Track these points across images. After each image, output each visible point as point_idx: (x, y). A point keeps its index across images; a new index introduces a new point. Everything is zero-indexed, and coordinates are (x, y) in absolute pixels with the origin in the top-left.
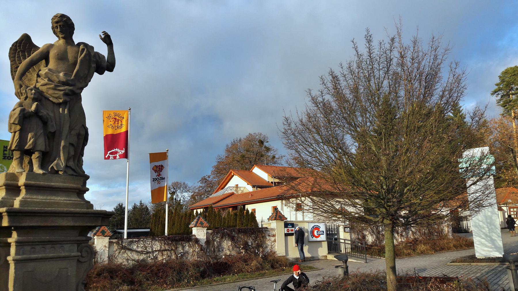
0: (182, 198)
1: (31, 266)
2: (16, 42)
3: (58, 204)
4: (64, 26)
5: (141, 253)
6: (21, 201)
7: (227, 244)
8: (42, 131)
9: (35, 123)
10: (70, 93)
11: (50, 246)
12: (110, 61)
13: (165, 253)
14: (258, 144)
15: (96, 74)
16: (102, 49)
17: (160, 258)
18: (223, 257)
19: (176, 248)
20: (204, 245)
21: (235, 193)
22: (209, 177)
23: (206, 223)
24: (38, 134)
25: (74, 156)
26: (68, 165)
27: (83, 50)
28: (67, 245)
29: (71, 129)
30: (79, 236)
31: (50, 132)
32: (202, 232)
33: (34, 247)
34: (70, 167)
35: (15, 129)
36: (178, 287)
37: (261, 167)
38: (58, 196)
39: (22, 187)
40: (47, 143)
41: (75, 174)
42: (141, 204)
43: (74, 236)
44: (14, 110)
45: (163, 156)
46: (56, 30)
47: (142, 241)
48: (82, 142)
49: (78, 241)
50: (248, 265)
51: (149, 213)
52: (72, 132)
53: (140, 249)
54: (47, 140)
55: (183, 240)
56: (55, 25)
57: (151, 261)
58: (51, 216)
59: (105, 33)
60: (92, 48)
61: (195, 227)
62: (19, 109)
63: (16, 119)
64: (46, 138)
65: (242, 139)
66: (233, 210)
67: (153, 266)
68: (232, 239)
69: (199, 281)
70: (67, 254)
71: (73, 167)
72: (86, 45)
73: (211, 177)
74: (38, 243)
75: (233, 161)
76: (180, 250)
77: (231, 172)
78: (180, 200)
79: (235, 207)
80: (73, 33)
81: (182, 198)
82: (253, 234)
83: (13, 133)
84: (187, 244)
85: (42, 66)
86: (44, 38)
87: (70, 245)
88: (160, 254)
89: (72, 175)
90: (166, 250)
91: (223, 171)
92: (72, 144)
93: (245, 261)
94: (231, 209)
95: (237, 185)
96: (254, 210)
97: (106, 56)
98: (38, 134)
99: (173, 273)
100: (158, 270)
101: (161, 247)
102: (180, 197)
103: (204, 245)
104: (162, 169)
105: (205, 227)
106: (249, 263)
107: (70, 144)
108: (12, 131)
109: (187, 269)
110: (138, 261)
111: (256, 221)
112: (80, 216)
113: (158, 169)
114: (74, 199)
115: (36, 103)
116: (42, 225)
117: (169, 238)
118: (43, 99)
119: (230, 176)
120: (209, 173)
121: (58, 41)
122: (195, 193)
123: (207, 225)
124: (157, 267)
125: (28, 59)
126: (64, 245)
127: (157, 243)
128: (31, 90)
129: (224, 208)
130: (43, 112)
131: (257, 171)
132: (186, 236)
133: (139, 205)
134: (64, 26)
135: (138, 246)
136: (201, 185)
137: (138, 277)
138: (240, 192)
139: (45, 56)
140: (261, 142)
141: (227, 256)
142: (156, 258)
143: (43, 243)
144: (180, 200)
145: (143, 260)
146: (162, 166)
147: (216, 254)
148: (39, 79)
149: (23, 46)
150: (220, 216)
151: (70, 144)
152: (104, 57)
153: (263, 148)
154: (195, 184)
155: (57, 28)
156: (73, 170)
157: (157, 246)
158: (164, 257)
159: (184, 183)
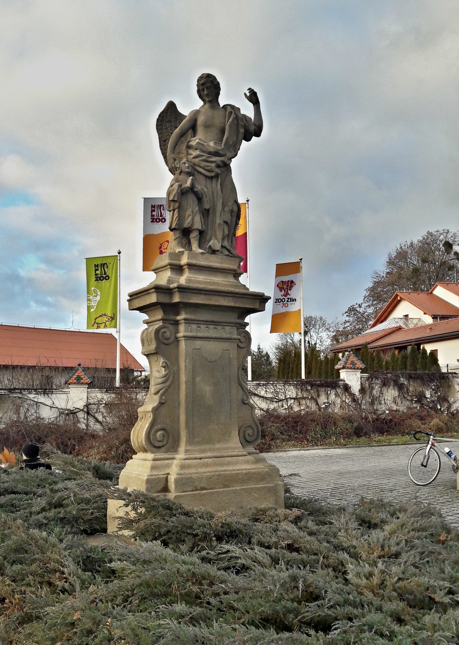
0: (318, 342)
1: (198, 344)
2: (163, 112)
3: (217, 284)
4: (209, 87)
5: (271, 400)
6: (186, 280)
7: (391, 393)
8: (197, 208)
9: (191, 200)
10: (221, 164)
11: (213, 326)
12: (257, 124)
13: (303, 402)
14: (443, 248)
15: (243, 141)
16: (248, 110)
17: (296, 409)
18: (387, 412)
19: (319, 396)
20: (357, 393)
21: (403, 326)
22: (360, 306)
23: (360, 364)
24: (195, 211)
25: (228, 235)
26: (223, 245)
27: (231, 113)
28: (228, 327)
29: (224, 205)
30: (238, 318)
31: (205, 209)
32: (355, 376)
33: (199, 325)
34: (225, 247)
35: (173, 206)
36: (323, 445)
37: (447, 286)
38: (217, 276)
39: (184, 267)
40: (203, 221)
41: (230, 255)
42: (259, 349)
43: (233, 318)
44: (171, 186)
45: (295, 267)
46: (202, 93)
47: (272, 384)
48: (235, 219)
49: (238, 323)
50: (425, 424)
51: (270, 364)
52: (226, 209)
53: (269, 395)
54: (202, 219)
55: (328, 386)
56: (201, 88)
57: (284, 411)
58: (214, 295)
59: (251, 90)
60: (239, 109)
61: (344, 368)
62: (177, 185)
63: (175, 195)
64: (202, 216)
65: (415, 242)
66: (399, 352)
67: (288, 416)
68: (400, 387)
69: (352, 440)
70: (228, 336)
71: (228, 248)
72: (233, 107)
73: (364, 305)
74: (202, 322)
75: (399, 278)
76: (322, 399)
77: (397, 295)
78: (315, 344)
79: (401, 347)
80: (219, 94)
81: (318, 342)
82: (432, 381)
83: (172, 212)
84: (333, 392)
85: (189, 136)
86: (190, 104)
87: (230, 327)
88: (296, 403)
89: (228, 255)
90: (304, 398)
91: (385, 296)
92: (226, 222)
93: (422, 418)
94: (396, 352)
95: (406, 316)
96: (434, 354)
97: (253, 118)
98: (195, 211)
99: (316, 427)
100: (295, 422)
101: (297, 394)
102: (315, 339)
103: (357, 393)
104: (291, 287)
105: (358, 369)
106: (427, 421)
107: (224, 222)
108: (171, 209)
109: (335, 423)
110: (267, 411)
111: (438, 365)
112: (240, 297)
113: (285, 287)
114: (231, 279)
115: (191, 177)
116: (207, 302)
117: (307, 383)
118: (196, 173)
119: (396, 301)
120: (360, 300)
121: (204, 106)
122: (338, 331)
123: (363, 366)
124: (293, 418)
125: (177, 130)
126: (225, 327)
127: (292, 387)
128: (185, 163)
129: (385, 349)
130: (198, 188)
131: (440, 291)
132: (332, 382)
133: (256, 350)
134: (209, 87)
135: (266, 391)
136: (347, 319)
137: (269, 429)
138: (411, 326)
139: (193, 127)
140: (448, 246)
141: (392, 411)
142: (291, 408)
143: (207, 322)
144: (315, 344)
145: (274, 409)
146: (292, 282)
147: (375, 408)
148: (191, 151)
149: (169, 117)
150: (380, 360)
151: (224, 222)
152: (251, 119)
153: (452, 255)
154: (339, 318)
155: (204, 90)
156: (228, 250)
157: (292, 392)
158: (302, 408)
159: (321, 319)
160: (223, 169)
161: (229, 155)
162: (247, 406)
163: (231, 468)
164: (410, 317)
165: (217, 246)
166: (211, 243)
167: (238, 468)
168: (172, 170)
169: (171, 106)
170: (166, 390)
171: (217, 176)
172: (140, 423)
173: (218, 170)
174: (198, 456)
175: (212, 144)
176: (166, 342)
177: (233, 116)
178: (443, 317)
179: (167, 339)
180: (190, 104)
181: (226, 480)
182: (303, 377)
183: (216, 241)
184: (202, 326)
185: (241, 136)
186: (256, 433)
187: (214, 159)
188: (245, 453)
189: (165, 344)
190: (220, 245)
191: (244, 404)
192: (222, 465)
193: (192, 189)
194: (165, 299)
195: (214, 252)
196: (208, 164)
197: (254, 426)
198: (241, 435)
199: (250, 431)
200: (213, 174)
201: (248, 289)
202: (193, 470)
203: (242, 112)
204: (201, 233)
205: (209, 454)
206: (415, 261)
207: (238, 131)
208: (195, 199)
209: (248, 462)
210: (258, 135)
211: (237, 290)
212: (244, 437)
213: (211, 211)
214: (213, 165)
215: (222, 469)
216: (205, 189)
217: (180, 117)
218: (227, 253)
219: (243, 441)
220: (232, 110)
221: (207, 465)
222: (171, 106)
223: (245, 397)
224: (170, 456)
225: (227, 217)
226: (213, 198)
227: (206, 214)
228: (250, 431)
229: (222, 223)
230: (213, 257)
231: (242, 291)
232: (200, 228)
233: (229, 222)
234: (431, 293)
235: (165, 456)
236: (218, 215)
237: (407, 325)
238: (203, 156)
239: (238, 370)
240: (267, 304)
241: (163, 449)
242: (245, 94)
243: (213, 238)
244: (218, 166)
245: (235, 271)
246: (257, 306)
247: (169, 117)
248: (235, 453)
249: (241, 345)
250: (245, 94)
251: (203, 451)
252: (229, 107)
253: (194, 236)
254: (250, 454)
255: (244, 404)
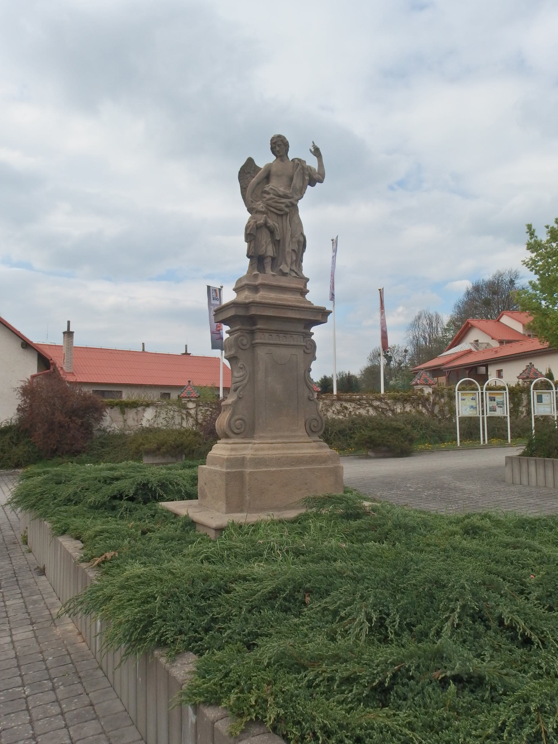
4: (279, 145)
8: (270, 239)
15: (309, 187)
16: (312, 162)
21: (473, 349)
24: (268, 242)
30: (304, 328)
34: (293, 271)
43: (300, 328)
48: (301, 248)
52: (293, 240)
60: (305, 162)
71: (296, 271)
72: (299, 160)
86: (265, 159)
92: (294, 250)
95: (477, 341)
98: (268, 242)
114: (299, 297)
118: (269, 212)
119: (467, 328)
130: (271, 222)
143: (278, 332)
156: (296, 273)
160: (291, 208)
161: (296, 197)
162: (313, 402)
163: (297, 452)
164: (479, 342)
165: (287, 270)
166: (281, 267)
167: (303, 452)
168: (250, 210)
169: (250, 161)
170: (243, 387)
171: (286, 214)
172: (223, 415)
173: (287, 210)
174: (270, 441)
175: (282, 189)
176: (244, 347)
177: (300, 167)
178: (509, 342)
179: (244, 345)
180: (265, 159)
181: (293, 461)
182: (459, 445)
183: (285, 265)
184: (273, 334)
185: (307, 182)
186: (320, 424)
187: (283, 200)
188: (310, 440)
189: (241, 349)
190: (289, 269)
191: (311, 400)
192: (289, 449)
193: (265, 225)
194: (241, 312)
195: (284, 274)
196: (278, 205)
197: (318, 418)
198: (308, 427)
199: (315, 423)
200: (282, 213)
201: (313, 304)
202: (266, 452)
203: (308, 164)
204: (273, 259)
205: (279, 440)
206: (486, 295)
207: (304, 179)
208: (268, 232)
209: (312, 448)
210: (321, 182)
211: (303, 305)
212: (310, 427)
213: (281, 241)
214: (283, 206)
215: (290, 452)
216: (277, 225)
217: (257, 169)
218: (294, 275)
219: (309, 430)
220: (299, 163)
221: (277, 449)
222: (250, 161)
223: (311, 395)
224: (246, 441)
225: (295, 247)
226: (283, 231)
227: (277, 243)
228: (315, 423)
229: (291, 251)
230: (284, 279)
231: (307, 305)
232: (272, 255)
233: (296, 250)
234: (498, 321)
235: (243, 441)
236: (287, 245)
237: (477, 349)
238: (274, 198)
239: (305, 372)
240: (329, 317)
241: (239, 436)
242: (311, 150)
243: (283, 263)
244: (287, 206)
245: (301, 289)
246: (319, 318)
247: (248, 170)
248: (301, 440)
249: (307, 351)
250: (311, 150)
251: (275, 438)
252: (296, 160)
253: (268, 261)
254: (314, 442)
255: (311, 400)
